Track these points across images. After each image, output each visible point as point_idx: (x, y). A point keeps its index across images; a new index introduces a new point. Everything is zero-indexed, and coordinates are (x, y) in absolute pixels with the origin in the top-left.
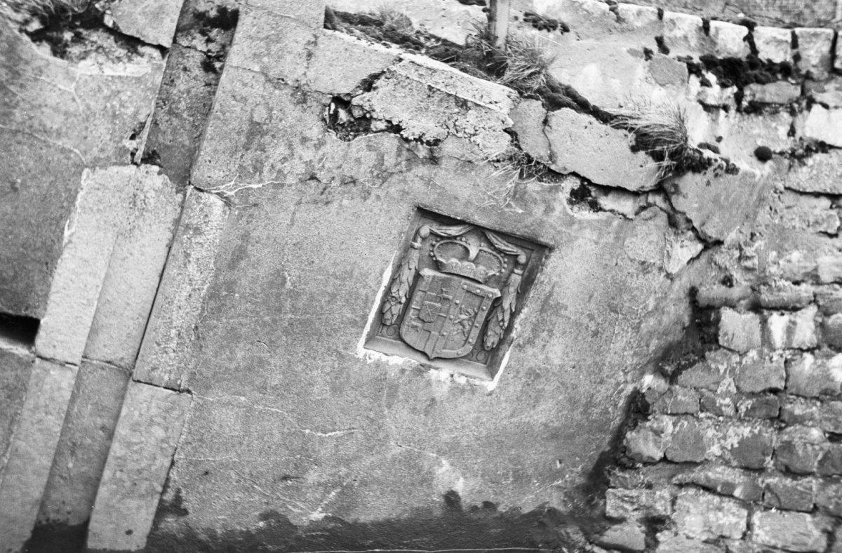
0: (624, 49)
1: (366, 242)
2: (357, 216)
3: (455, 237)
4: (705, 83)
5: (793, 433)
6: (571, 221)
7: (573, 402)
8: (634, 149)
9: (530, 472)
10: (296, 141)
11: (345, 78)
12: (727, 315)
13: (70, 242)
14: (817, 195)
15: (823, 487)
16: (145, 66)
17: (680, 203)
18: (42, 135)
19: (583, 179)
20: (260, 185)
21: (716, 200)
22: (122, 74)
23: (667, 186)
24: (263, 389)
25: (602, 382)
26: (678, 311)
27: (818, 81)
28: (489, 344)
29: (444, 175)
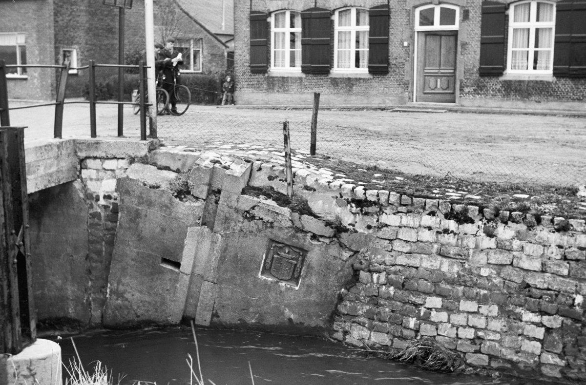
1: (258, 248)
2: (254, 241)
4: (351, 207)
5: (381, 309)
6: (312, 244)
7: (321, 295)
8: (326, 226)
9: (312, 314)
10: (237, 222)
12: (362, 273)
14: (386, 239)
15: (390, 326)
17: (342, 241)
21: (353, 240)
23: (337, 236)
24: (235, 284)
25: (329, 290)
26: (348, 271)
29: (275, 231)
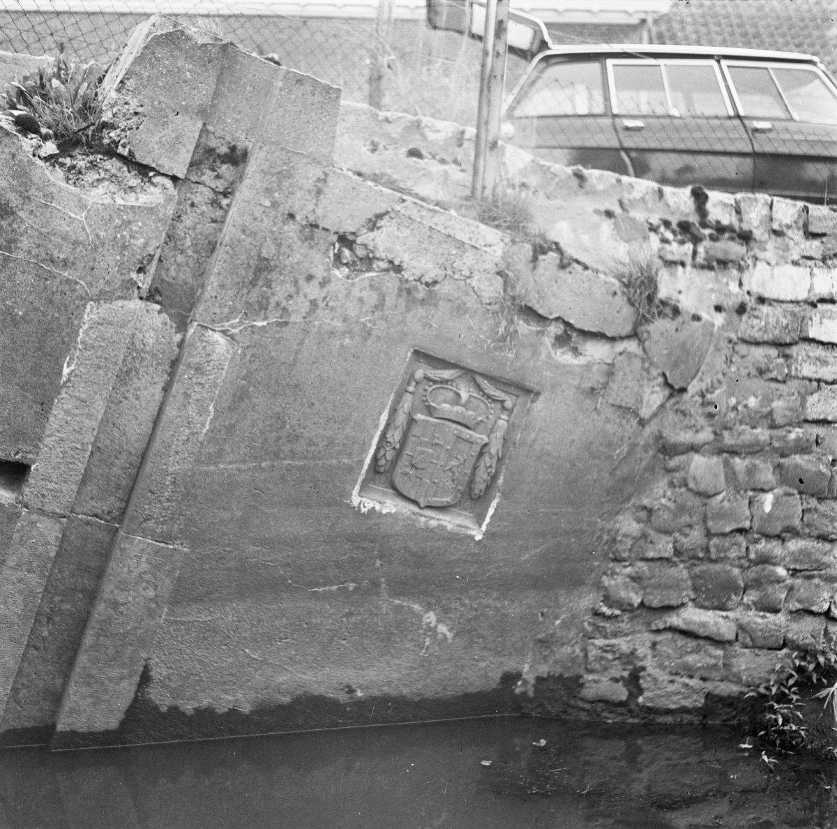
0: (590, 210)
3: (447, 382)
11: (352, 216)
13: (69, 380)
16: (154, 195)
18: (48, 266)
19: (567, 324)
20: (265, 323)
22: (134, 204)
27: (761, 242)
28: (477, 491)
